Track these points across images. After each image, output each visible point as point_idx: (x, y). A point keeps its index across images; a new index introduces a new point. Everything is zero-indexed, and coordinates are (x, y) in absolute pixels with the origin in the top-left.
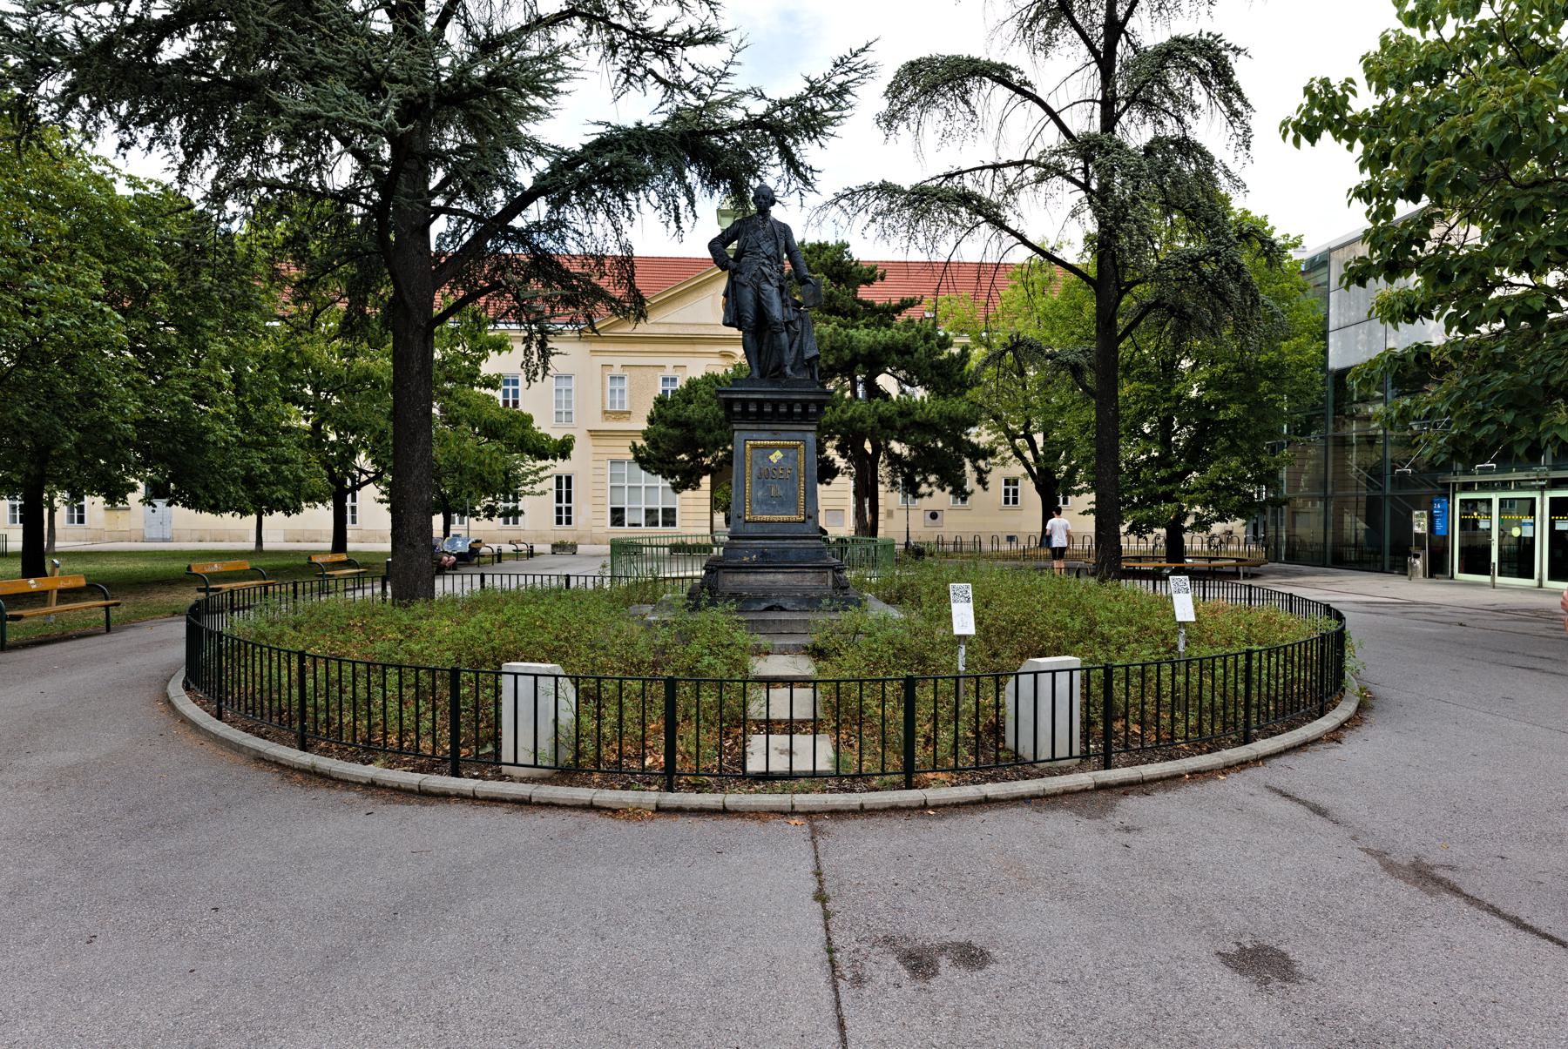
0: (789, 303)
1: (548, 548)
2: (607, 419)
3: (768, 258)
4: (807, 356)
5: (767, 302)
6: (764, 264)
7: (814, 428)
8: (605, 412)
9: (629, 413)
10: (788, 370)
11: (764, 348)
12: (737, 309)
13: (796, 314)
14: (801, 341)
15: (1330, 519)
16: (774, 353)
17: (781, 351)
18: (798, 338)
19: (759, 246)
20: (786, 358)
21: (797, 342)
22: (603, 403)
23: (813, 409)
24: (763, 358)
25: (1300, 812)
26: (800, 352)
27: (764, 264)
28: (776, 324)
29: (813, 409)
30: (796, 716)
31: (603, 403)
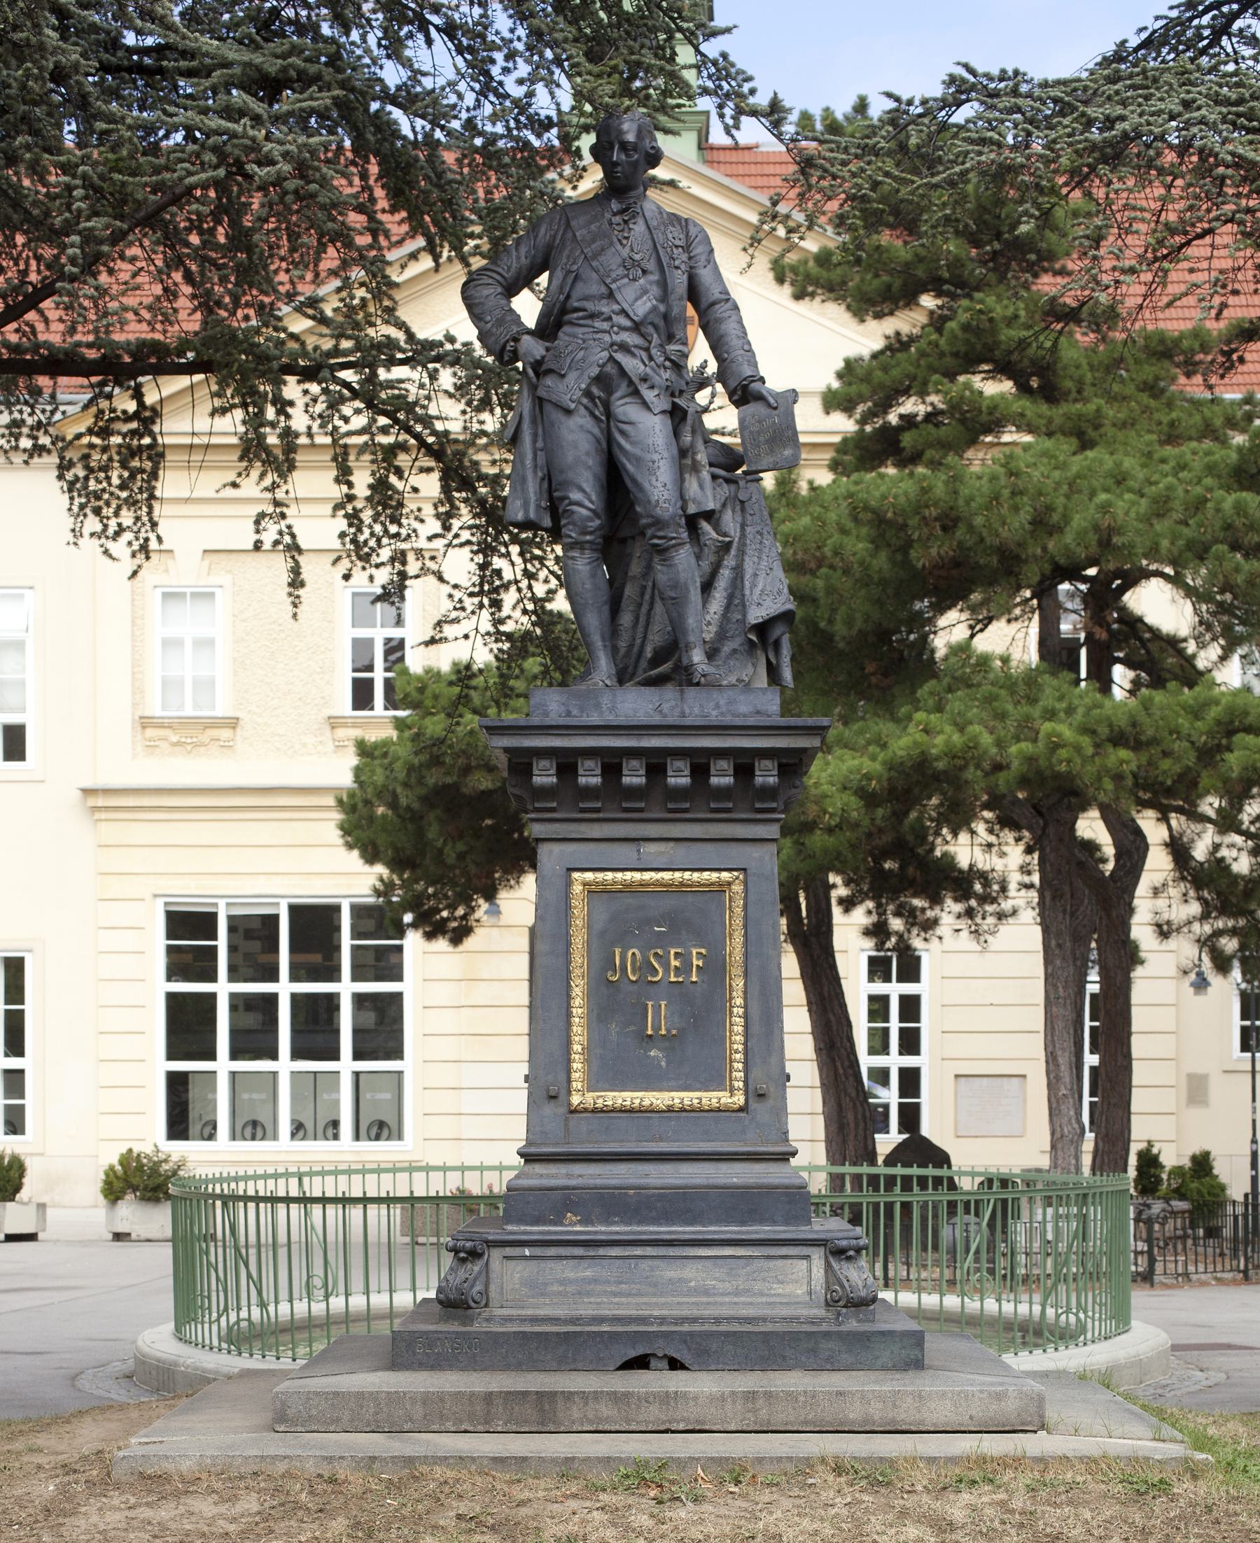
0: (702, 457)
1: (653, 1363)
2: (151, 747)
3: (637, 327)
4: (756, 615)
5: (638, 461)
6: (624, 348)
7: (773, 831)
8: (146, 723)
9: (232, 723)
10: (697, 656)
11: (630, 591)
12: (549, 477)
13: (725, 490)
14: (738, 571)
15: (619, 1229)
16: (659, 608)
17: (676, 605)
18: (730, 561)
19: (611, 295)
20: (691, 621)
21: (725, 574)
22: (138, 690)
23: (766, 775)
24: (626, 619)
25: (674, 1427)
26: (736, 599)
27: (624, 348)
28: (658, 523)
29: (766, 775)
30: (168, 1233)
31: (138, 690)
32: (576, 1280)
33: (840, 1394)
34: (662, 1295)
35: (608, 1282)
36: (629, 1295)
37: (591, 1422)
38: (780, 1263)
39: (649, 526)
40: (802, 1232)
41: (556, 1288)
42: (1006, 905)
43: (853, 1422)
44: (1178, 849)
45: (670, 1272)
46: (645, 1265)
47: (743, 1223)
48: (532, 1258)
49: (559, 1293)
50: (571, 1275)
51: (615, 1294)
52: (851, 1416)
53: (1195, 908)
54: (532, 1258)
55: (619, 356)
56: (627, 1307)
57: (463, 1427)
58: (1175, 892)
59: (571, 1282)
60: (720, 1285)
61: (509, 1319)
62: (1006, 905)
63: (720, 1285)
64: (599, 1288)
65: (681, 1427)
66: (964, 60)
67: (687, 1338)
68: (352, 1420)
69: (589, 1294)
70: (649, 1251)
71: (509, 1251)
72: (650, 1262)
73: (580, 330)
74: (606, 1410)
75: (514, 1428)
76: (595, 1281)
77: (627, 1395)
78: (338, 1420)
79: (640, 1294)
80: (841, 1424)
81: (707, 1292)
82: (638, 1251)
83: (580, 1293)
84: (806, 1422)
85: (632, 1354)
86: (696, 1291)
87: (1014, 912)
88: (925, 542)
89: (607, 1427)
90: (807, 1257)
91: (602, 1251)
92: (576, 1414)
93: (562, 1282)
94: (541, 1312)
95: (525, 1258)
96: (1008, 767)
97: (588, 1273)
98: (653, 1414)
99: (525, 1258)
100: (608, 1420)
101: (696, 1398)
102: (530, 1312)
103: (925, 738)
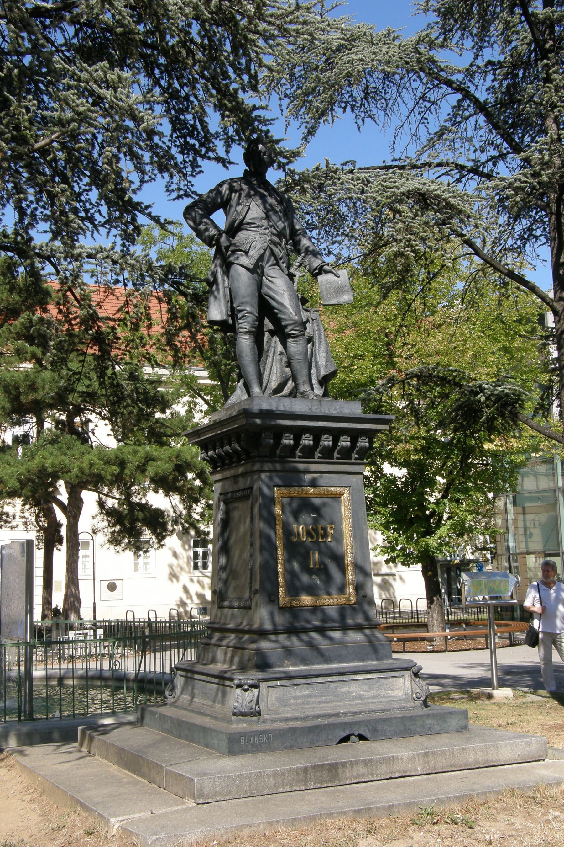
32: (301, 697)
33: (463, 749)
34: (342, 700)
35: (316, 696)
36: (326, 702)
37: (355, 778)
38: (391, 680)
39: (290, 325)
40: (387, 663)
41: (292, 701)
42: (13, 524)
43: (470, 764)
44: (101, 504)
45: (344, 689)
46: (333, 685)
47: (363, 660)
48: (281, 686)
49: (294, 704)
50: (299, 694)
51: (319, 702)
52: (470, 760)
53: (106, 523)
54: (281, 686)
55: (272, 246)
56: (327, 709)
57: (294, 788)
58: (99, 518)
59: (299, 697)
60: (366, 694)
61: (273, 721)
62: (13, 524)
63: (366, 694)
64: (313, 700)
65: (397, 775)
66: (225, 169)
67: (367, 723)
68: (238, 792)
69: (308, 703)
70: (335, 678)
71: (270, 683)
72: (334, 684)
73: (252, 233)
74: (361, 770)
75: (319, 785)
76: (310, 696)
77: (371, 760)
78: (230, 792)
79: (331, 701)
80: (465, 765)
81: (361, 698)
82: (330, 679)
83: (303, 703)
84: (451, 766)
85: (344, 735)
86: (355, 698)
87: (17, 526)
88: (27, 394)
89: (363, 780)
90: (402, 676)
91: (313, 680)
92: (348, 774)
93: (295, 698)
94: (288, 715)
95: (277, 686)
96: (69, 471)
97: (307, 692)
98: (383, 770)
99: (277, 686)
100: (363, 775)
101: (402, 759)
102: (282, 716)
103: (43, 460)
